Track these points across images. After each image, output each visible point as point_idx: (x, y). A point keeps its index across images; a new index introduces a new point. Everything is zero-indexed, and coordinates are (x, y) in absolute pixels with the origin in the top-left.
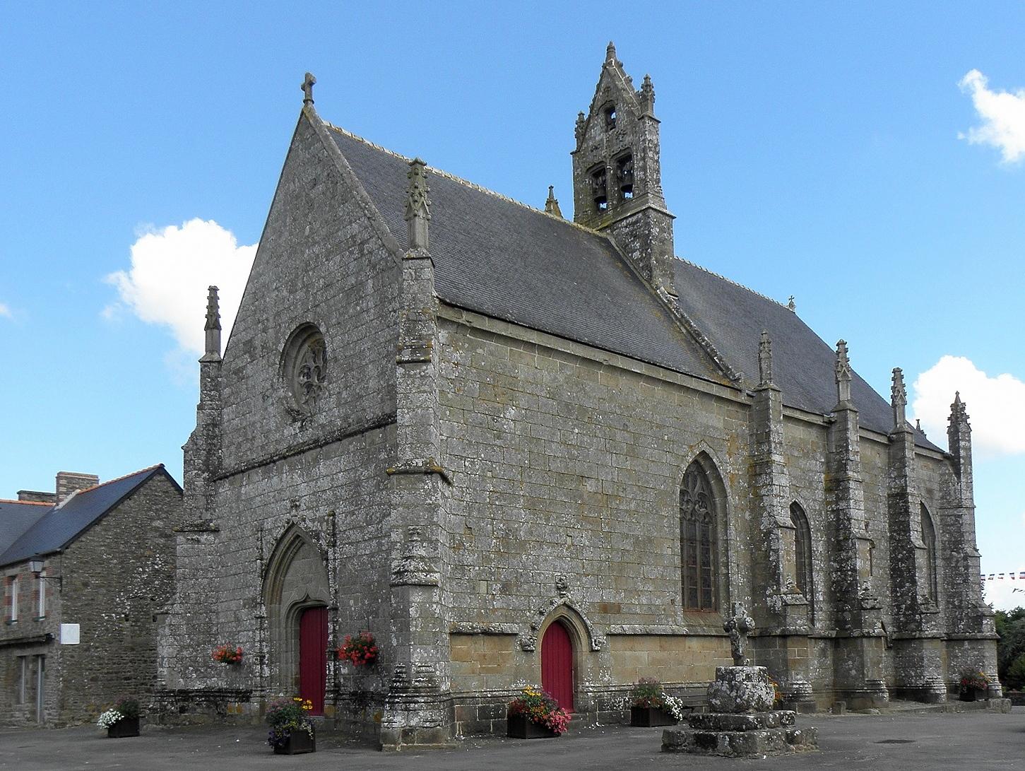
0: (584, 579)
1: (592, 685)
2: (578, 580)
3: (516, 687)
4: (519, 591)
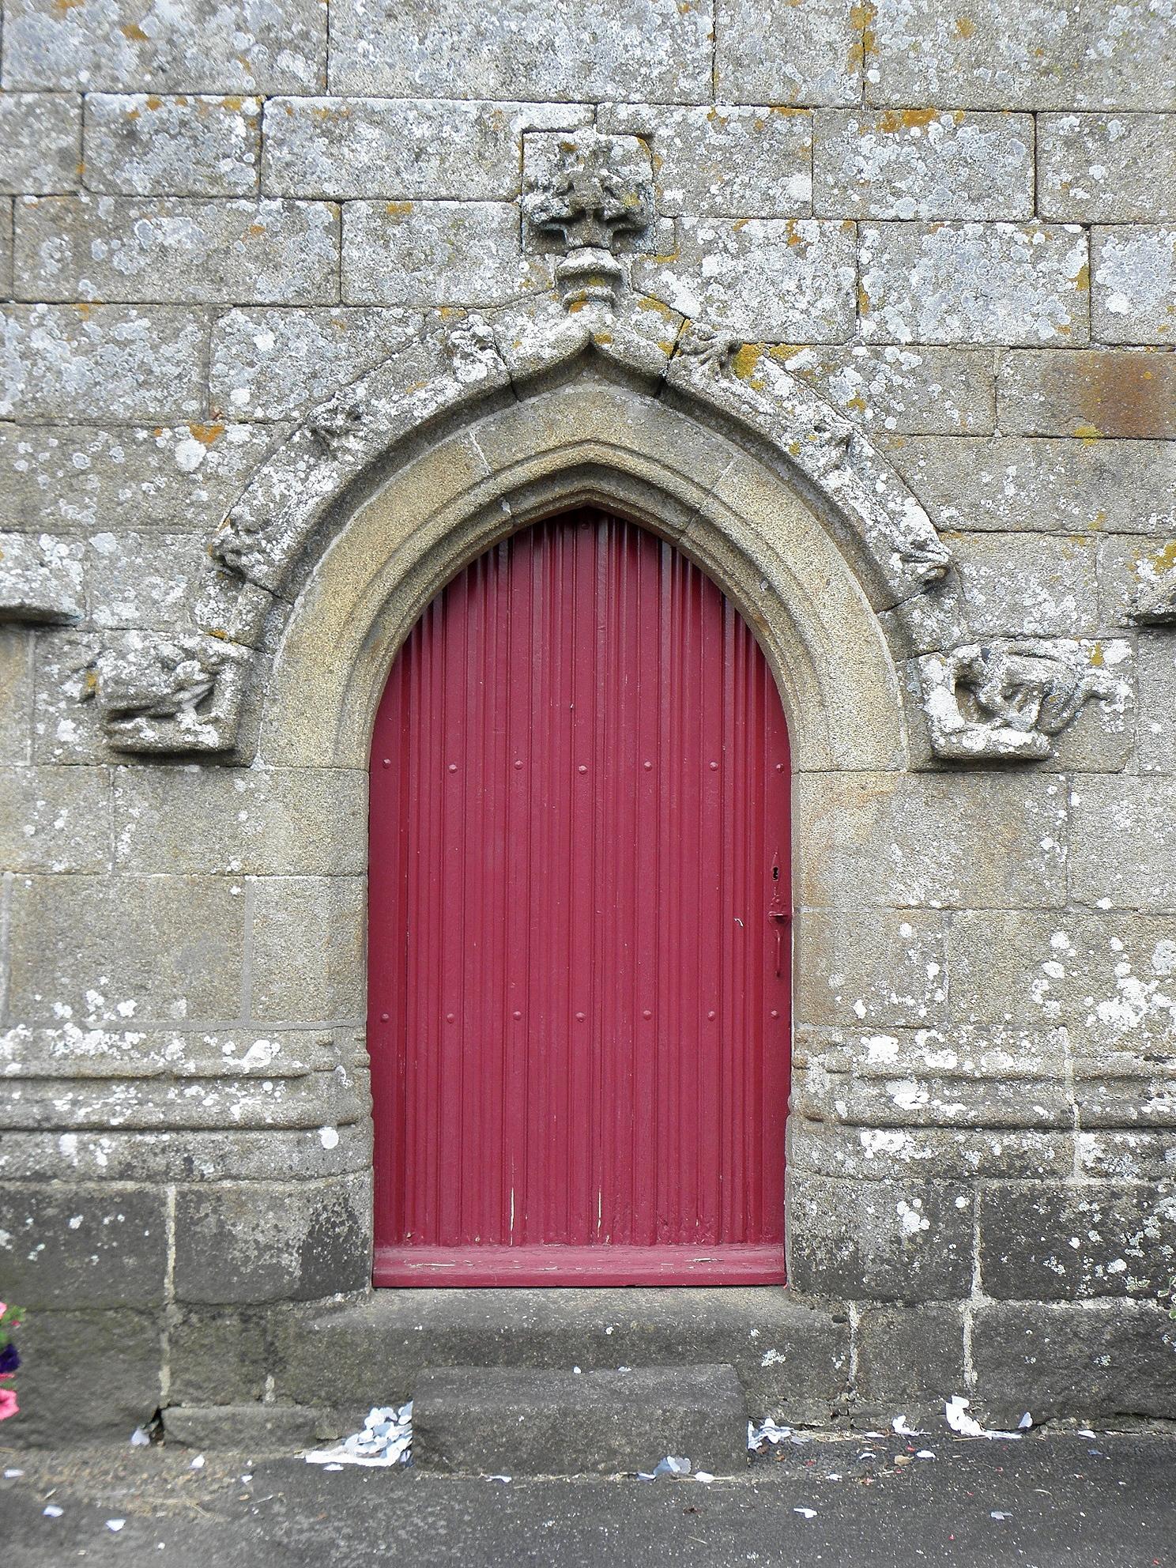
0: (871, 153)
1: (947, 1061)
2: (791, 160)
3: (31, 1049)
4: (104, 271)
